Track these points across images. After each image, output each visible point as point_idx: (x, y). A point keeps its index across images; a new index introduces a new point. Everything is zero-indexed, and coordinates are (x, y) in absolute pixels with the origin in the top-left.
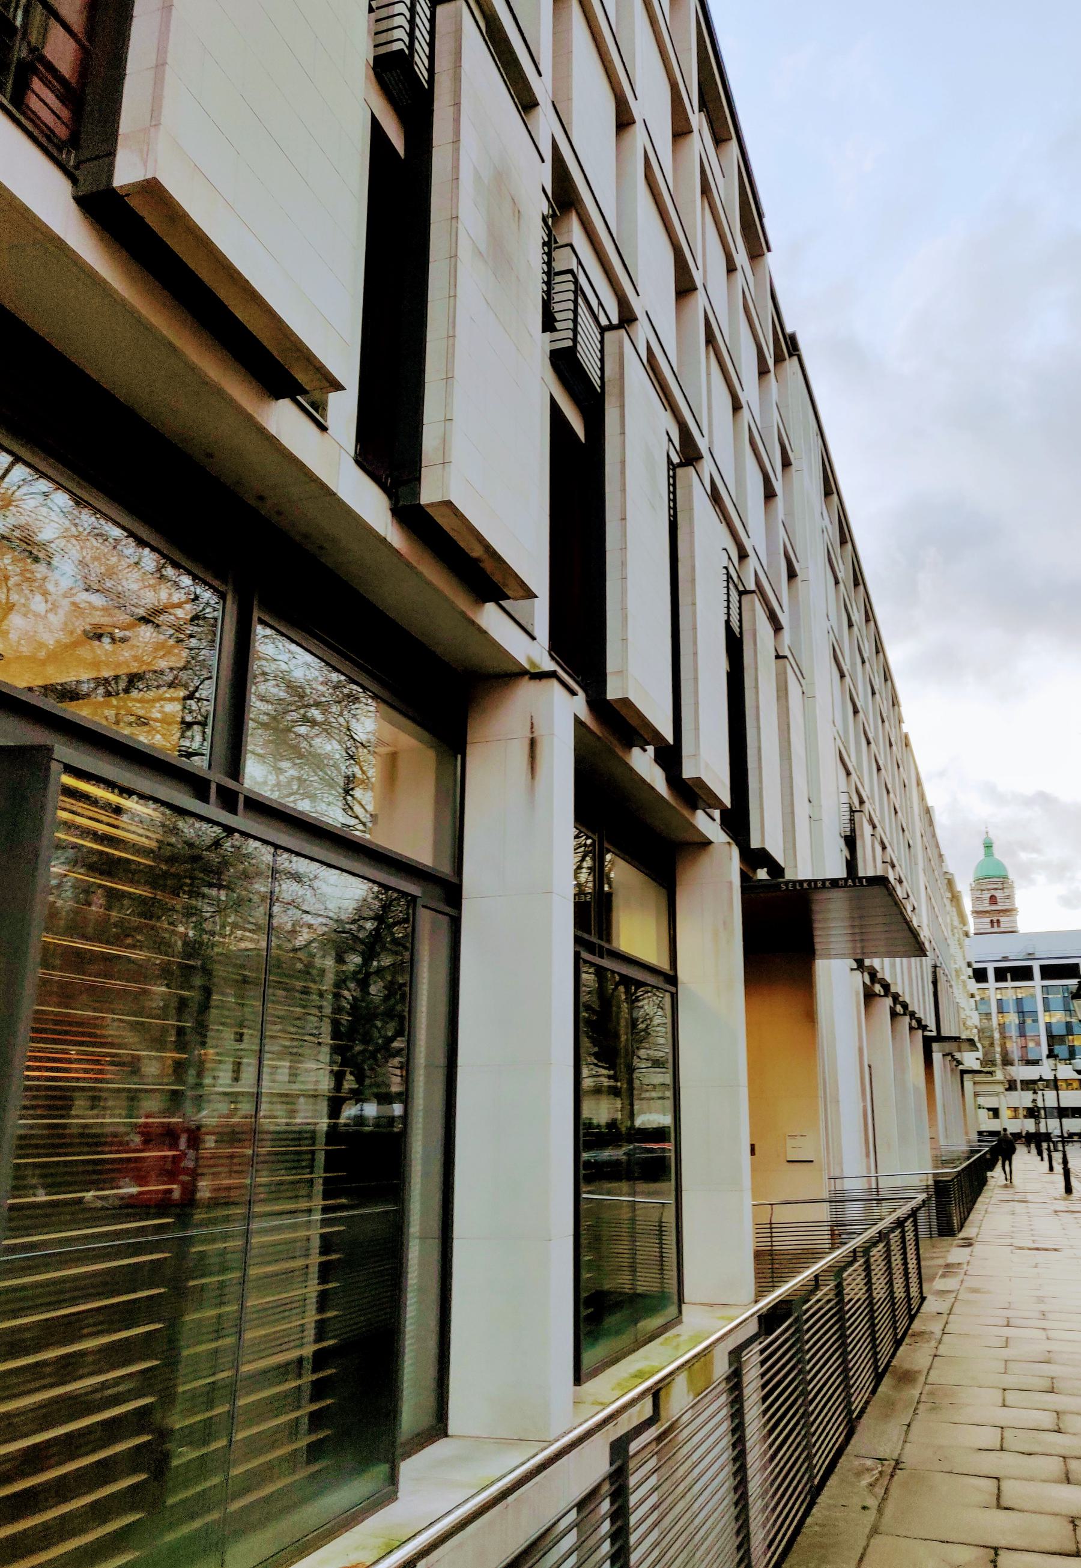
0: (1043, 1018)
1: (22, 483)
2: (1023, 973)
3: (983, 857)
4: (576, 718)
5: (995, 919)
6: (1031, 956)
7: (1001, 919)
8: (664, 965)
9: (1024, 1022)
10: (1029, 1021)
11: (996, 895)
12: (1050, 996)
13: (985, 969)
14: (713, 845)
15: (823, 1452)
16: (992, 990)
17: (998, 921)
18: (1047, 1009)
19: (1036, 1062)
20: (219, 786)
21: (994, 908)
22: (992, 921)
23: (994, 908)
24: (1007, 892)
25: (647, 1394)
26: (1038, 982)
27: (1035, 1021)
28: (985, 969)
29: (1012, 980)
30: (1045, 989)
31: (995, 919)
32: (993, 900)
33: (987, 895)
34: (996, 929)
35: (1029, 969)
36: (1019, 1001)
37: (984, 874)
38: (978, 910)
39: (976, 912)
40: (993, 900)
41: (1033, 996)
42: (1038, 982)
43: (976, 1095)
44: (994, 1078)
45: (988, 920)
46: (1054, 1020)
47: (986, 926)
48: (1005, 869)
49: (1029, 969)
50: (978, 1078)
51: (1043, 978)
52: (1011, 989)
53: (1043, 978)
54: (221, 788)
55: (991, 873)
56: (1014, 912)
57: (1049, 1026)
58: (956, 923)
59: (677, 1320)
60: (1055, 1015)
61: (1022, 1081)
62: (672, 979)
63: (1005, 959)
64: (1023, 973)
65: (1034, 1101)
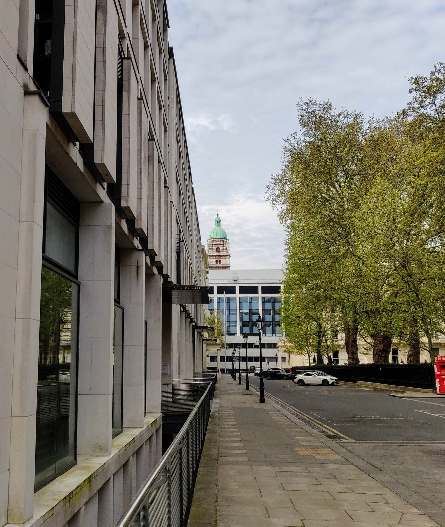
4: (47, 123)
5: (218, 260)
6: (236, 282)
7: (221, 260)
8: (71, 268)
13: (235, 287)
14: (103, 203)
15: (159, 511)
17: (220, 261)
19: (234, 334)
22: (217, 261)
24: (226, 246)
25: (121, 468)
26: (238, 295)
28: (235, 287)
29: (226, 293)
31: (218, 260)
32: (218, 250)
33: (215, 247)
34: (218, 265)
35: (257, 288)
40: (218, 250)
43: (207, 350)
44: (217, 343)
45: (215, 260)
47: (213, 263)
49: (257, 288)
50: (209, 343)
51: (263, 293)
53: (263, 293)
59: (74, 463)
62: (76, 277)
65: (233, 353)
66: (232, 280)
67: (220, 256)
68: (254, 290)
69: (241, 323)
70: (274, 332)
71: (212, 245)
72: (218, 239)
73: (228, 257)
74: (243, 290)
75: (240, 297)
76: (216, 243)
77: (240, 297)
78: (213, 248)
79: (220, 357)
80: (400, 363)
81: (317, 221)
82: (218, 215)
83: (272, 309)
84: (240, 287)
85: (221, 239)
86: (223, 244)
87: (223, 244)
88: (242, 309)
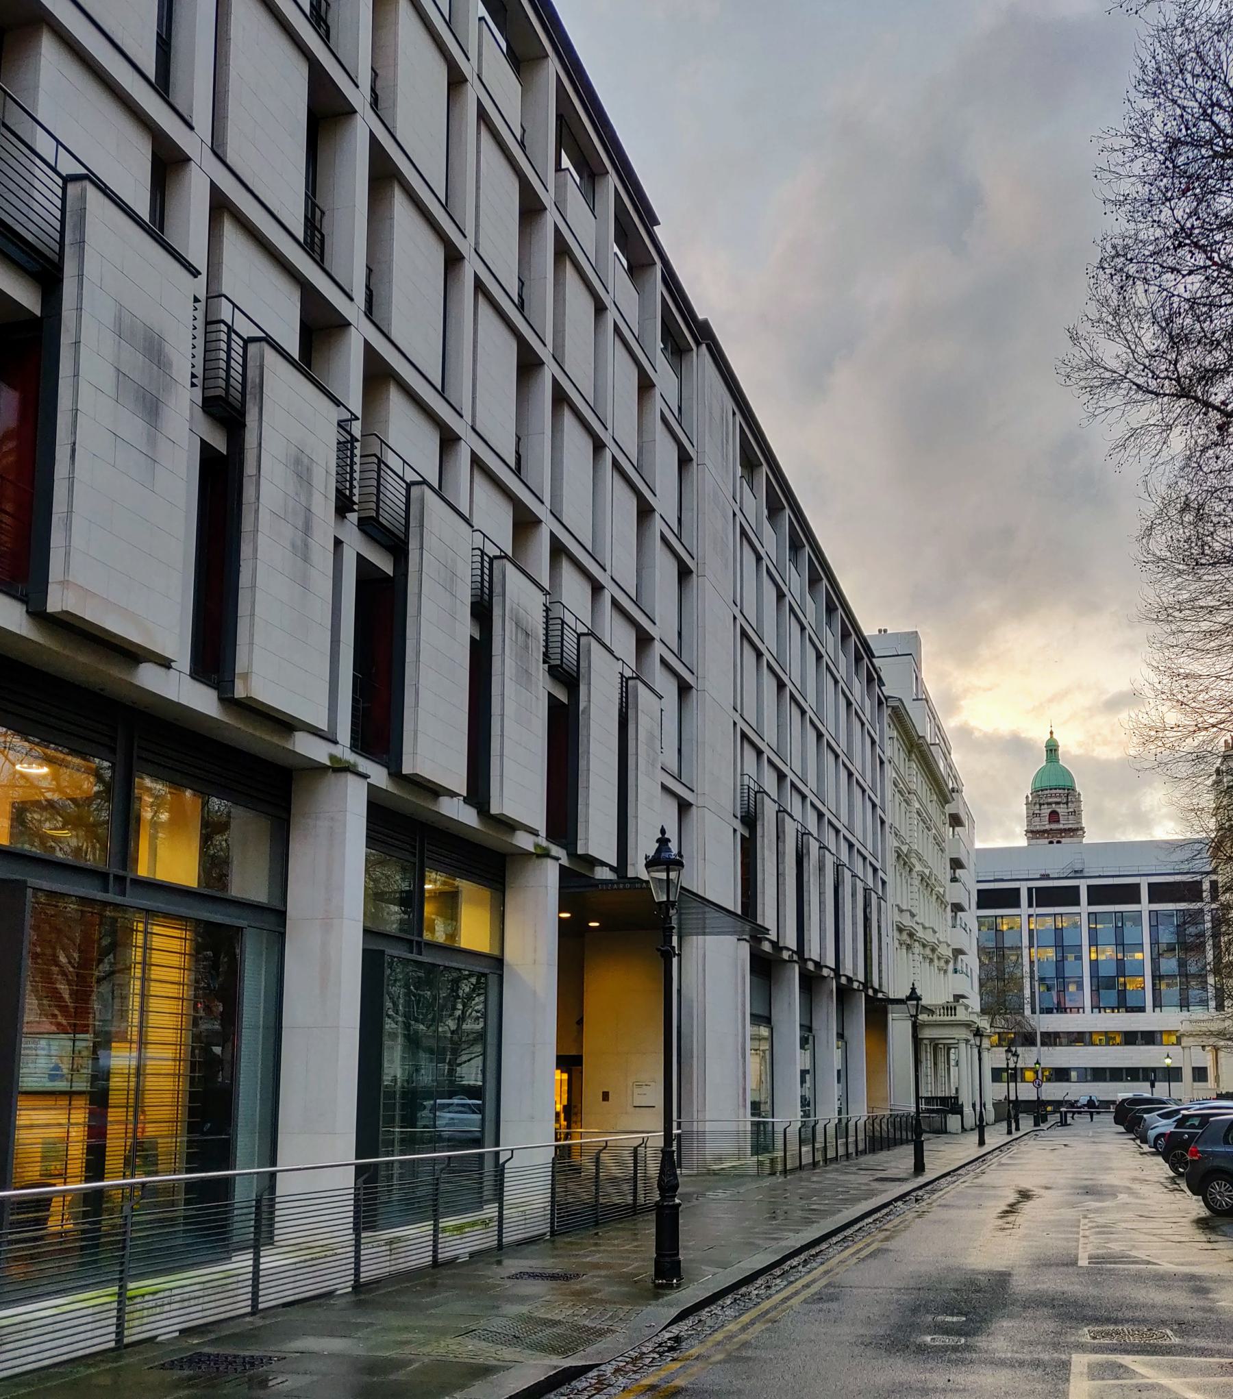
0: (1087, 955)
1: (917, 948)
2: (1068, 896)
3: (1044, 764)
9: (1063, 959)
10: (1071, 957)
11: (1059, 810)
12: (1098, 926)
16: (1025, 918)
18: (1094, 942)
20: (115, 876)
21: (1054, 826)
23: (1054, 826)
24: (1072, 808)
26: (1084, 908)
27: (1079, 958)
30: (1092, 917)
32: (1054, 816)
33: (1046, 811)
36: (1058, 931)
37: (1046, 784)
38: (1034, 829)
39: (1032, 832)
40: (1054, 816)
41: (1077, 926)
42: (1084, 908)
44: (957, 1018)
46: (1102, 957)
48: (1073, 781)
52: (1046, 919)
54: (116, 877)
55: (1054, 784)
56: (1080, 832)
57: (1094, 964)
58: (933, 808)
60: (1104, 952)
61: (1042, 1034)
63: (1045, 877)
64: (1068, 896)
66: (1069, 871)
67: (1061, 831)
68: (1129, 893)
69: (1095, 980)
70: (1184, 1004)
71: (1038, 806)
72: (1054, 791)
73: (1080, 832)
74: (1099, 895)
75: (1089, 914)
76: (1050, 800)
77: (1089, 914)
78: (1043, 811)
79: (993, 1069)
80: (419, 1115)
81: (1169, 86)
82: (1051, 733)
83: (1178, 943)
84: (1089, 887)
85: (1061, 791)
86: (1067, 803)
87: (1067, 803)
88: (1097, 945)
